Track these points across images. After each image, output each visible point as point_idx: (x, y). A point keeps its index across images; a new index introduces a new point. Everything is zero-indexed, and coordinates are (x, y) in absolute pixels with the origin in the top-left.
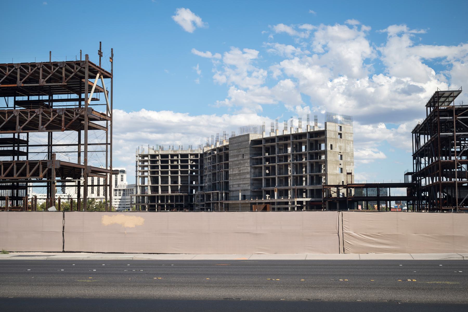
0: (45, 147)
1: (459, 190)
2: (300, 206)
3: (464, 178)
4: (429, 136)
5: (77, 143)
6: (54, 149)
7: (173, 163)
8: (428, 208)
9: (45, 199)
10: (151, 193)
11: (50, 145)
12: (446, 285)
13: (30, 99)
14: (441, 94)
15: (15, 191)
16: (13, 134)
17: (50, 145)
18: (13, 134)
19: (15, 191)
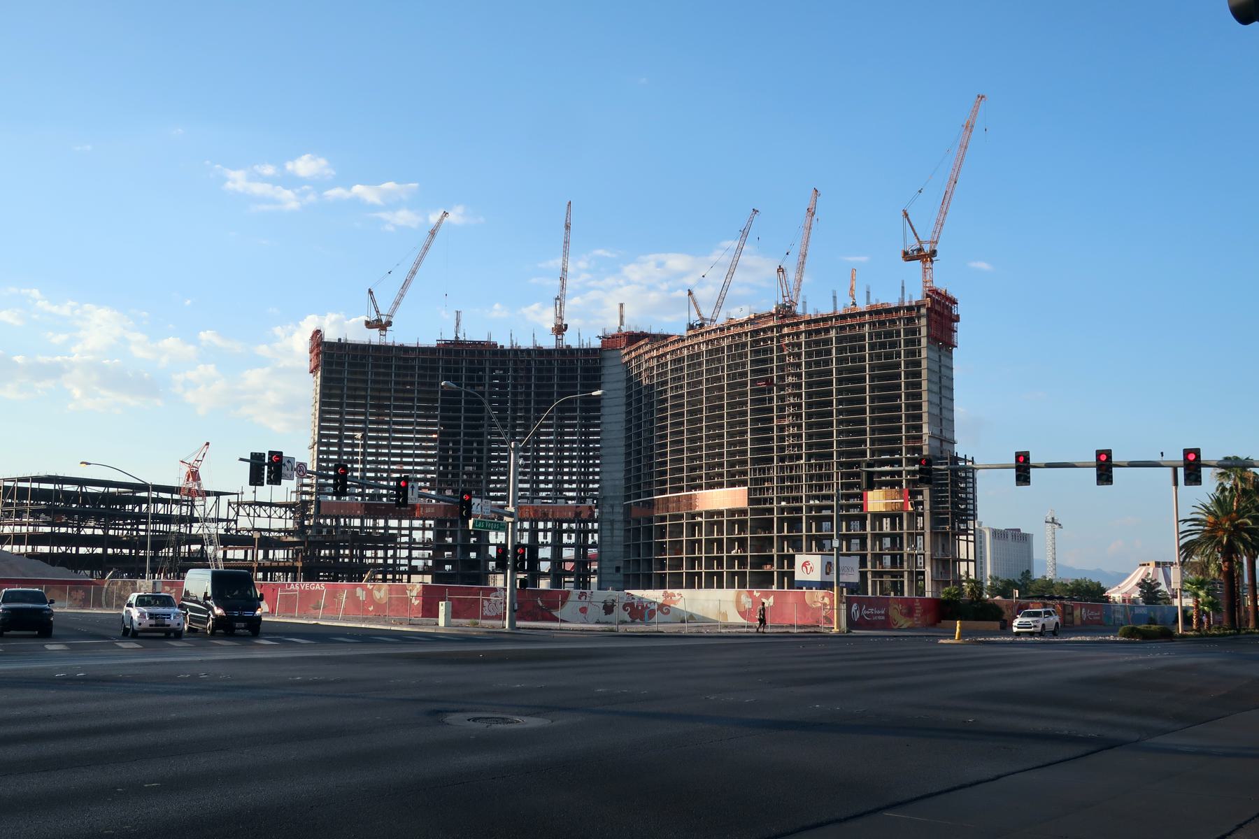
0: (636, 327)
1: (873, 560)
2: (397, 477)
3: (427, 519)
4: (372, 520)
5: (966, 563)
6: (610, 527)
7: (1177, 607)
8: (381, 500)
9: (940, 535)
10: (432, 582)
11: (612, 536)
12: (740, 388)
13: (95, 533)
14: (780, 544)
15: (117, 531)
16: (495, 547)
17: (612, 536)
18: (495, 547)
19: (117, 531)
